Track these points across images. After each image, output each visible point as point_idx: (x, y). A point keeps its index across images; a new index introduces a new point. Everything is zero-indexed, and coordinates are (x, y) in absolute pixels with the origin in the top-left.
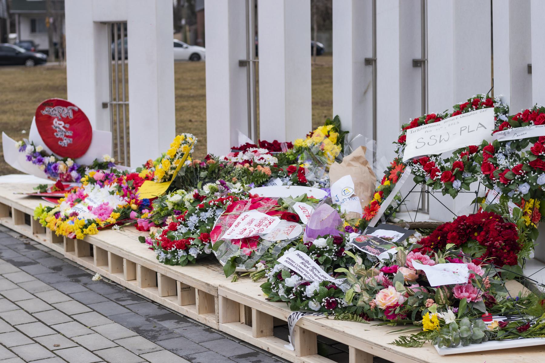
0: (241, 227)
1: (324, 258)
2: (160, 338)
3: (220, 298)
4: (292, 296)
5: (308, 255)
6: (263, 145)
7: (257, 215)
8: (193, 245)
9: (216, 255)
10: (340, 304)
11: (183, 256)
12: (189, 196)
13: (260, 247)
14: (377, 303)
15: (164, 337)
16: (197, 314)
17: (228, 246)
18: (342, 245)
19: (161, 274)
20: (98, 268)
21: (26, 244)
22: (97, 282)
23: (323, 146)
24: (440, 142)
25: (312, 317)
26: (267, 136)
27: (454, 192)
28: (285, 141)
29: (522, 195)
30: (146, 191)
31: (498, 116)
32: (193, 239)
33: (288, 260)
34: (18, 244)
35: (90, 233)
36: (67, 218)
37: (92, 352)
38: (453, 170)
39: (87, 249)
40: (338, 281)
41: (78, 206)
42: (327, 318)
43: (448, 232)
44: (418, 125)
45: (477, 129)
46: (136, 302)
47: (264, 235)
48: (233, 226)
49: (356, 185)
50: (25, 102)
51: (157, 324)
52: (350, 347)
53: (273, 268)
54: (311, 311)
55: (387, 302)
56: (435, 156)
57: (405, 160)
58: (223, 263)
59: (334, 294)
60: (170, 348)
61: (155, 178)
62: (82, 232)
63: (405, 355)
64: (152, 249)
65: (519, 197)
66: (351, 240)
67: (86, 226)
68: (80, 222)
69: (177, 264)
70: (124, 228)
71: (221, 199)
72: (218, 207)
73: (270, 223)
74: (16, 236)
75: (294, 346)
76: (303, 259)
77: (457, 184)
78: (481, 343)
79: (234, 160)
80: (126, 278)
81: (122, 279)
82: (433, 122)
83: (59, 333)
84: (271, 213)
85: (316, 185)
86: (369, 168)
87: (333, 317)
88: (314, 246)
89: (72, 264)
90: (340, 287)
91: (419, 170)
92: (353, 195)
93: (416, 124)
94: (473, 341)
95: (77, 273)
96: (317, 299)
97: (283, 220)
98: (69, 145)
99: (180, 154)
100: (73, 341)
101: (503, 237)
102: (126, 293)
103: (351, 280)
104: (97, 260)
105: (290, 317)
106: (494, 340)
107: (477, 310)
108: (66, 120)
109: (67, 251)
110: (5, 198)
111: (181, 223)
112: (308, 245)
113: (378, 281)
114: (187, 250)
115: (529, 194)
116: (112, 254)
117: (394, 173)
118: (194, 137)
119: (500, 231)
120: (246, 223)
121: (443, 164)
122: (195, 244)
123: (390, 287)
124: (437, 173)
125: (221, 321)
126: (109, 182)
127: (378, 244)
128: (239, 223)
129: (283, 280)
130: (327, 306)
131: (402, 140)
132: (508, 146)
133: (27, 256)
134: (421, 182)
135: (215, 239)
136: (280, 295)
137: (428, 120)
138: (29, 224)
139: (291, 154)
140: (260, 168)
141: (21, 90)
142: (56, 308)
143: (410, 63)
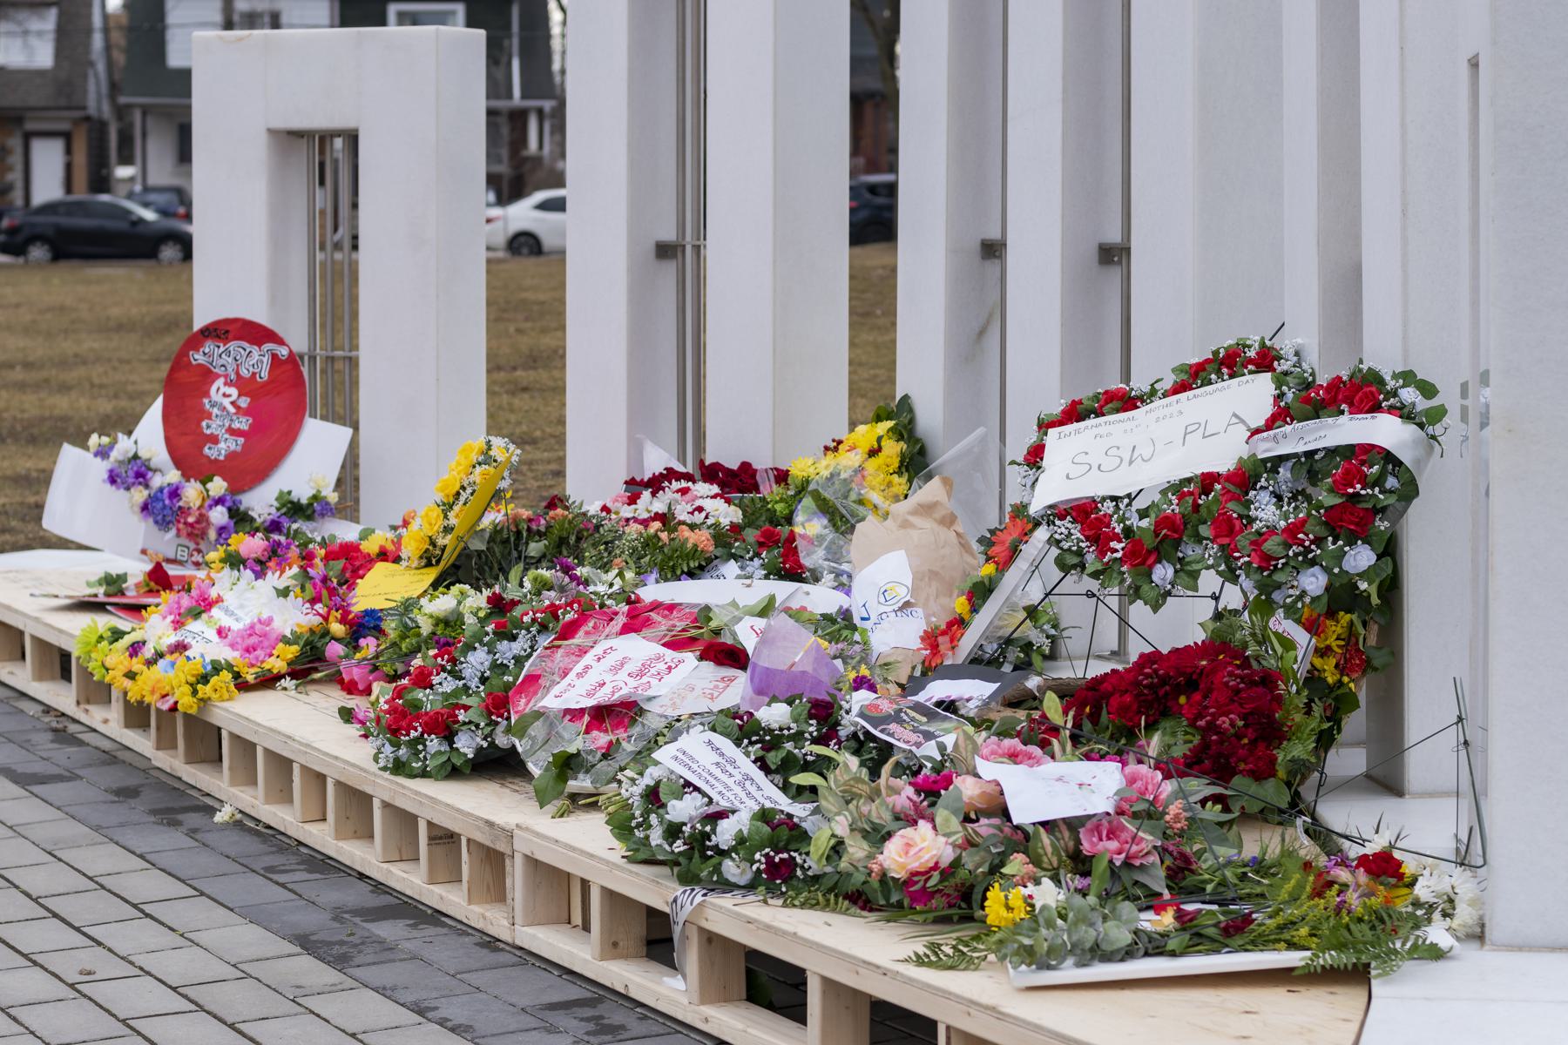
0: (593, 678)
2: (357, 961)
3: (518, 859)
4: (679, 846)
5: (738, 745)
6: (711, 473)
7: (640, 648)
8: (465, 723)
9: (520, 749)
10: (802, 867)
11: (439, 753)
12: (477, 600)
13: (636, 730)
14: (886, 864)
15: (370, 959)
17: (552, 726)
18: (832, 720)
19: (383, 802)
20: (234, 790)
21: (55, 730)
22: (225, 826)
24: (1131, 463)
25: (726, 901)
26: (724, 451)
27: (1153, 594)
28: (771, 465)
29: (1307, 600)
30: (377, 590)
31: (1283, 394)
32: (466, 708)
33: (680, 755)
34: (35, 730)
35: (214, 696)
36: (160, 655)
37: (174, 989)
39: (205, 740)
40: (799, 810)
41: (194, 626)
42: (765, 902)
43: (1112, 694)
44: (1080, 419)
45: (1213, 431)
46: (318, 876)
47: (650, 699)
48: (572, 675)
49: (918, 577)
50: (128, 362)
51: (356, 927)
53: (641, 774)
54: (727, 886)
56: (1114, 499)
57: (1035, 508)
58: (535, 771)
59: (788, 842)
60: (377, 983)
61: (404, 555)
62: (195, 692)
63: (929, 986)
64: (366, 736)
65: (1300, 605)
66: (855, 710)
67: (204, 679)
68: (188, 666)
69: (424, 774)
70: (309, 687)
71: (552, 605)
72: (544, 628)
73: (670, 668)
74: (32, 709)
75: (684, 977)
76: (722, 755)
77: (1163, 573)
78: (1122, 960)
79: (627, 512)
80: (298, 814)
81: (289, 818)
82: (1118, 411)
83: (99, 944)
85: (828, 578)
87: (780, 902)
89: (170, 782)
90: (803, 825)
91: (1070, 534)
92: (907, 604)
93: (1074, 414)
94: (1098, 953)
95: (177, 804)
96: (742, 853)
97: (705, 663)
98: (231, 456)
99: (469, 490)
100: (131, 963)
101: (1241, 705)
102: (298, 853)
104: (231, 768)
105: (675, 901)
106: (1161, 954)
107: (1144, 886)
109: (158, 748)
110: (9, 608)
111: (443, 669)
112: (741, 718)
113: (898, 808)
114: (449, 737)
117: (1003, 543)
118: (512, 447)
119: (1237, 691)
120: (609, 665)
121: (1134, 521)
122: (470, 722)
123: (921, 822)
124: (1113, 544)
125: (518, 920)
127: (924, 719)
128: (587, 668)
129: (663, 806)
130: (765, 871)
131: (1035, 456)
132: (1284, 472)
133: (56, 758)
134: (1074, 567)
135: (521, 706)
136: (653, 843)
137: (1107, 402)
138: (69, 680)
139: (782, 500)
140: (685, 532)
141: (120, 328)
142: (103, 887)
143: (1093, 253)
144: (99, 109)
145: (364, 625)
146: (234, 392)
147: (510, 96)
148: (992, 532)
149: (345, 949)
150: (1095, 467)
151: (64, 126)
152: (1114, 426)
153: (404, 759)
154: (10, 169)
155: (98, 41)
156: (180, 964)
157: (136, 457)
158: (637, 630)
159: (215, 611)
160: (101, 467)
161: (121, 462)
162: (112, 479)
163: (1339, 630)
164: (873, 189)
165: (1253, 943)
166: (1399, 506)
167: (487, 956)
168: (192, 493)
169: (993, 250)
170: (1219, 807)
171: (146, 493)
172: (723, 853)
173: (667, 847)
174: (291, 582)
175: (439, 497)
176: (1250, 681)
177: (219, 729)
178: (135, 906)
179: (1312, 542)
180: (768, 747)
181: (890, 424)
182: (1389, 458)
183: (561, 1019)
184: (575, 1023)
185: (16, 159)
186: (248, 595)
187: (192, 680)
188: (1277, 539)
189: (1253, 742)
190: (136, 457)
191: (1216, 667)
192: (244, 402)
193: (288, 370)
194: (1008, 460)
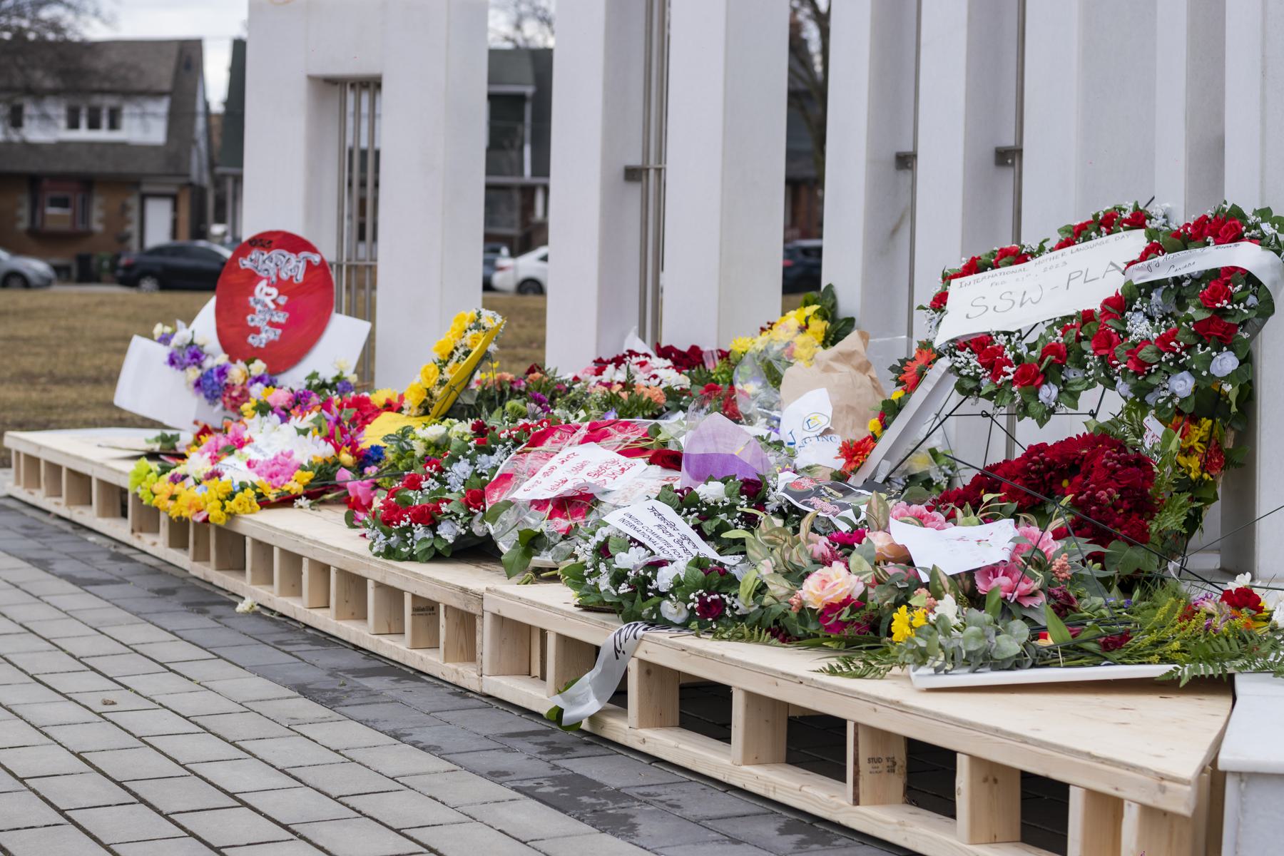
1: (716, 523)
4: (624, 589)
6: (664, 352)
8: (447, 514)
9: (492, 532)
10: (731, 608)
11: (425, 540)
16: (441, 662)
18: (760, 496)
22: (246, 614)
23: (792, 350)
24: (1022, 304)
25: (663, 635)
26: (677, 336)
27: (1039, 410)
28: (714, 348)
29: (1177, 401)
33: (627, 518)
35: (239, 509)
37: (187, 718)
38: (1042, 360)
39: (231, 547)
40: (729, 560)
41: (227, 460)
44: (978, 271)
45: (1091, 276)
47: (606, 492)
48: (539, 475)
52: (734, 689)
54: (659, 622)
55: (824, 593)
56: (1006, 333)
61: (405, 405)
62: (223, 507)
65: (1170, 405)
66: (781, 487)
67: (231, 496)
69: (412, 558)
77: (1048, 392)
78: (1010, 669)
82: (1011, 264)
84: (628, 453)
86: (872, 379)
88: (697, 495)
90: (734, 572)
92: (827, 431)
93: (973, 267)
98: (271, 344)
99: (462, 350)
101: (1117, 481)
103: (757, 555)
104: (252, 570)
108: (283, 286)
110: (80, 459)
111: (431, 476)
114: (433, 525)
115: (1192, 400)
116: (283, 551)
119: (1114, 470)
121: (1023, 350)
122: (452, 513)
123: (835, 563)
124: (1006, 369)
125: (486, 671)
126: (302, 411)
130: (699, 609)
131: (940, 302)
132: (1156, 297)
135: (495, 497)
136: (602, 589)
137: (1001, 257)
144: (200, 177)
145: (366, 458)
146: (274, 291)
147: (521, 173)
148: (903, 362)
149: (336, 694)
150: (991, 309)
151: (172, 190)
152: (1008, 275)
153: (394, 546)
154: (129, 222)
155: (200, 124)
156: (193, 702)
157: (191, 344)
158: (597, 441)
159: (246, 449)
160: (163, 352)
161: (180, 348)
162: (172, 361)
163: (1201, 433)
164: (806, 251)
165: (1129, 656)
166: (1257, 321)
167: (458, 702)
168: (237, 372)
169: (906, 161)
170: (1098, 565)
171: (198, 372)
172: (664, 595)
173: (613, 592)
174: (310, 425)
175: (436, 356)
176: (1126, 462)
177: (244, 537)
178: (162, 664)
179: (1182, 349)
180: (704, 517)
181: (816, 307)
182: (1250, 279)
183: (517, 743)
184: (530, 746)
185: (134, 215)
186: (274, 435)
187: (223, 496)
188: (1149, 348)
189: (1128, 512)
190: (191, 344)
191: (1094, 454)
192: (283, 300)
193: (319, 274)
194: (915, 306)
